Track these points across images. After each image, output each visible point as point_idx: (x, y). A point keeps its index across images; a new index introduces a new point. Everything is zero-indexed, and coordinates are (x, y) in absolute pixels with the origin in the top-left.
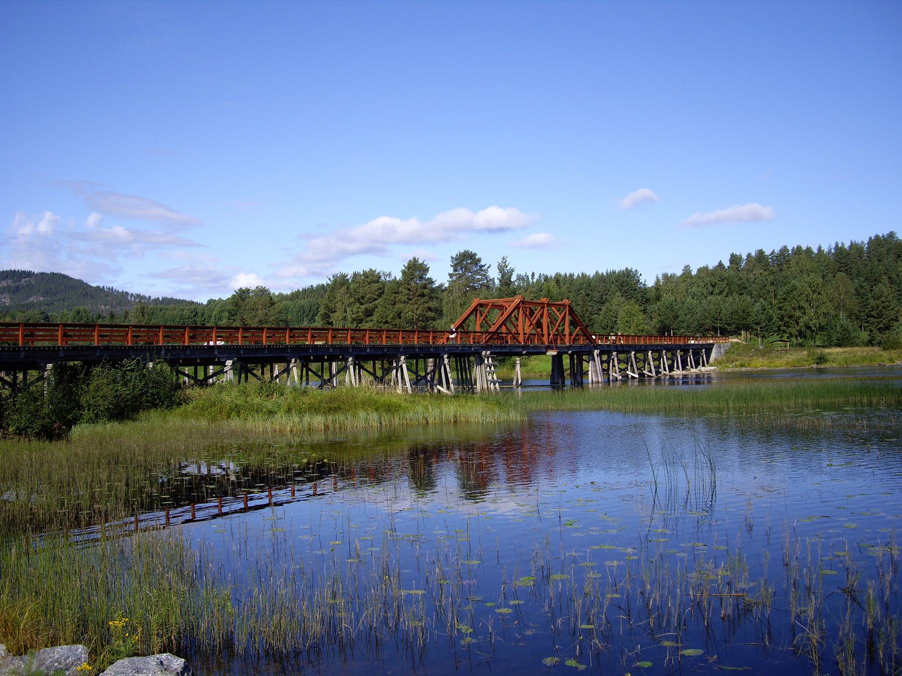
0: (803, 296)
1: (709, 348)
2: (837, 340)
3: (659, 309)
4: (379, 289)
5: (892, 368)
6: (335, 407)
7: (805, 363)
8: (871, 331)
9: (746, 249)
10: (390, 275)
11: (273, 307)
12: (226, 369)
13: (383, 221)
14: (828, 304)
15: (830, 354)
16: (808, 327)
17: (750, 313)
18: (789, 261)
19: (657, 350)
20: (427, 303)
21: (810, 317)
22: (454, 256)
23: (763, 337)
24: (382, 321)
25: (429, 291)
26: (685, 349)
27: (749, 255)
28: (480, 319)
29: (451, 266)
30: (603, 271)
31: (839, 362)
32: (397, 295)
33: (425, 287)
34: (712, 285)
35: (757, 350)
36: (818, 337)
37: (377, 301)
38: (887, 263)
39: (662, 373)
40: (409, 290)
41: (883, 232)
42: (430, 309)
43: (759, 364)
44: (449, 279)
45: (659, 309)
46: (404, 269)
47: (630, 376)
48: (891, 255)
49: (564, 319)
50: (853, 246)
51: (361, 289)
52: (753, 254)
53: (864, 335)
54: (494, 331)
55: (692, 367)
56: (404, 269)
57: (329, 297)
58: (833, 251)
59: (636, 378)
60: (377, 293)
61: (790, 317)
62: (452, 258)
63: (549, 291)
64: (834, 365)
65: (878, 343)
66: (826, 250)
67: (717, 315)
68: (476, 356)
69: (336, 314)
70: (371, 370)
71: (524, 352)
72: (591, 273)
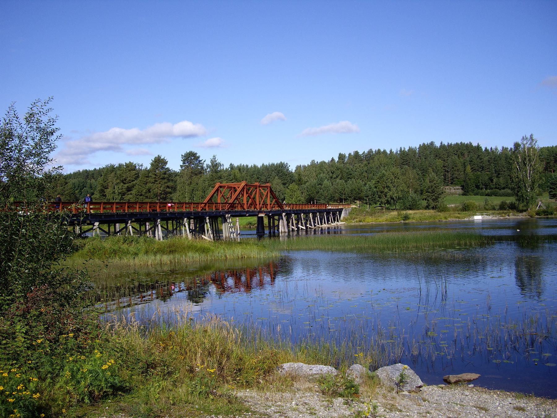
0: (389, 180)
1: (340, 211)
2: (409, 206)
3: (307, 187)
4: (135, 174)
5: (446, 222)
6: (173, 250)
7: (397, 220)
8: (428, 200)
9: (348, 151)
10: (142, 165)
11: (67, 185)
12: (95, 228)
13: (117, 130)
14: (404, 184)
15: (410, 214)
16: (392, 198)
17: (363, 191)
18: (373, 158)
19: (306, 213)
20: (166, 183)
21: (393, 193)
22: (184, 155)
23: (370, 204)
24: (138, 194)
25: (168, 176)
26: (328, 212)
27: (350, 154)
28: (220, 195)
29: (182, 161)
30: (266, 163)
31: (416, 219)
32: (148, 178)
33: (165, 173)
34: (331, 172)
35: (367, 212)
36: (397, 204)
37: (134, 182)
38: (430, 160)
39: (317, 226)
40: (155, 175)
41: (427, 142)
42: (168, 187)
43: (370, 220)
44: (180, 168)
45: (307, 187)
46: (152, 162)
47: (300, 228)
48: (432, 155)
49: (267, 196)
50: (410, 149)
51: (124, 174)
52: (352, 154)
53: (424, 203)
54: (232, 202)
55: (332, 222)
56: (152, 162)
57: (104, 179)
58: (399, 152)
59: (304, 229)
60: (134, 177)
61: (382, 192)
62: (182, 156)
63: (235, 176)
64: (414, 221)
65: (432, 208)
66: (395, 152)
67: (342, 191)
68: (222, 217)
69: (108, 190)
70: (166, 227)
71: (247, 215)
72: (259, 165)
